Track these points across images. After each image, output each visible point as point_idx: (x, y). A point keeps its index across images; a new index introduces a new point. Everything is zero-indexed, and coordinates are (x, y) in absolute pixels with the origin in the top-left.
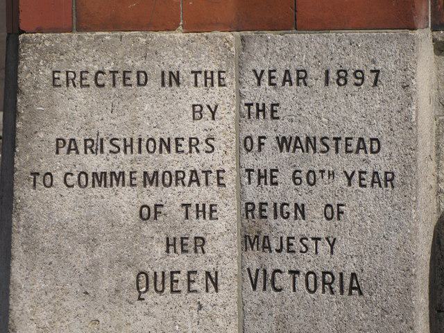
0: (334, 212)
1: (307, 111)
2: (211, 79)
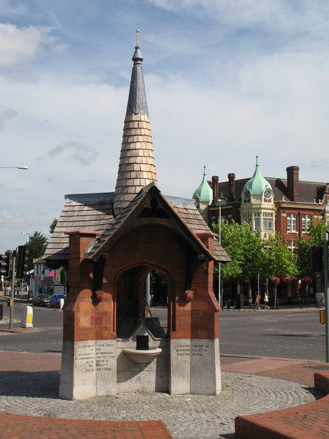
0: (107, 361)
1: (103, 349)
2: (93, 346)
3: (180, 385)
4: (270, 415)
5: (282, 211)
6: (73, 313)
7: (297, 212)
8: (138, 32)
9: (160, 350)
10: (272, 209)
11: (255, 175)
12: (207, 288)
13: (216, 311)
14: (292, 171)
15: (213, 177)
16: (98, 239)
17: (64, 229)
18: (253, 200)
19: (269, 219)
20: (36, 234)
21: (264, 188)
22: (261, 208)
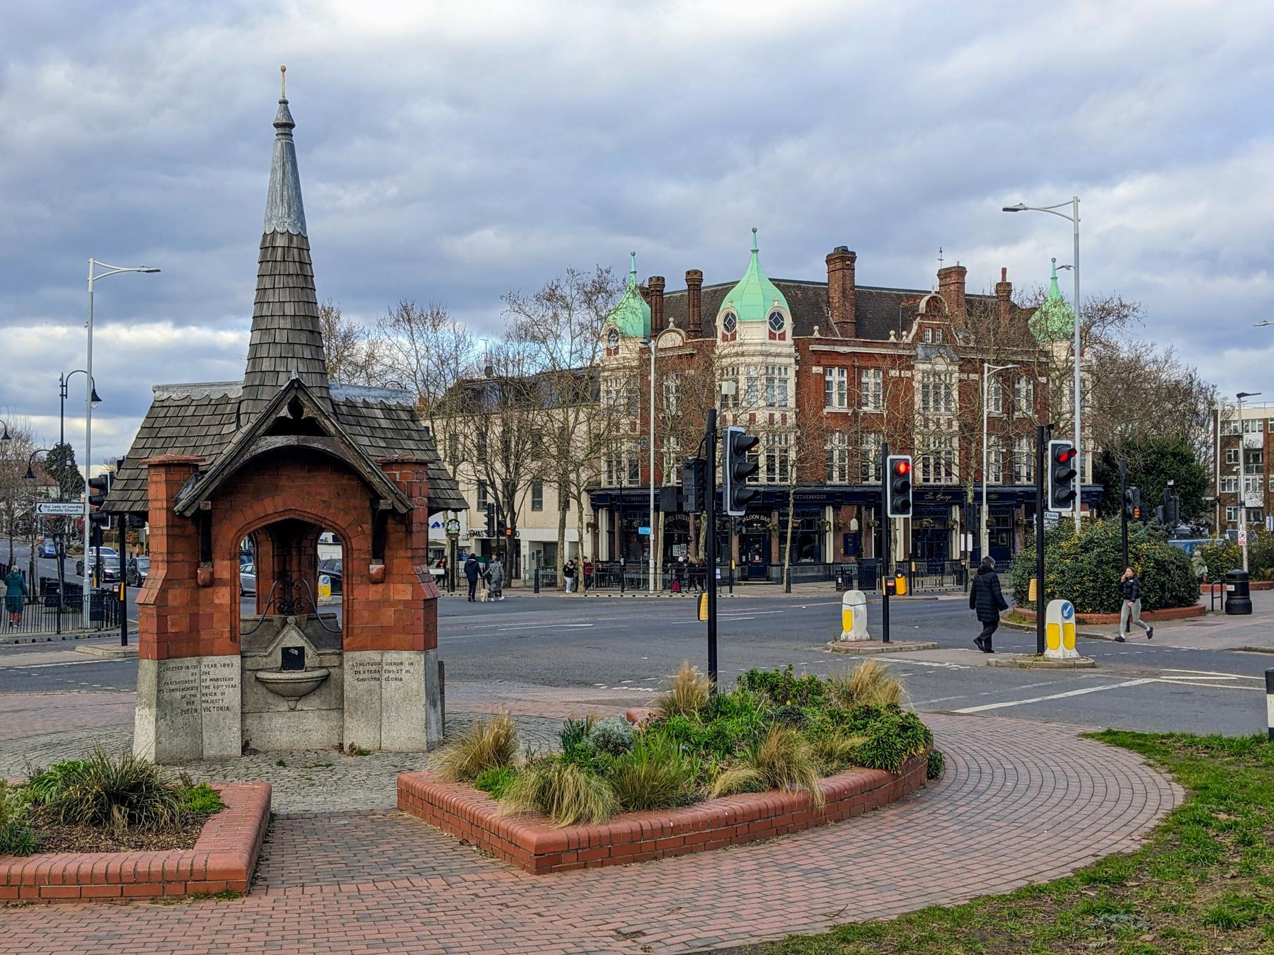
10: (789, 356)
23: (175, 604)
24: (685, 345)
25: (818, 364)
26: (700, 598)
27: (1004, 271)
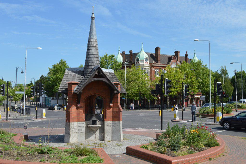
3: (108, 137)
4: (138, 146)
5: (153, 67)
6: (69, 112)
7: (159, 68)
8: (93, 7)
9: (101, 125)
10: (148, 66)
11: (141, 51)
12: (118, 103)
13: (121, 111)
14: (157, 49)
15: (123, 52)
16: (79, 85)
17: (65, 81)
18: (140, 63)
19: (147, 71)
20: (42, 76)
21: (145, 58)
22: (143, 66)
23: (73, 111)
24: (129, 64)
25: (154, 68)
26: (159, 111)
27: (186, 52)
